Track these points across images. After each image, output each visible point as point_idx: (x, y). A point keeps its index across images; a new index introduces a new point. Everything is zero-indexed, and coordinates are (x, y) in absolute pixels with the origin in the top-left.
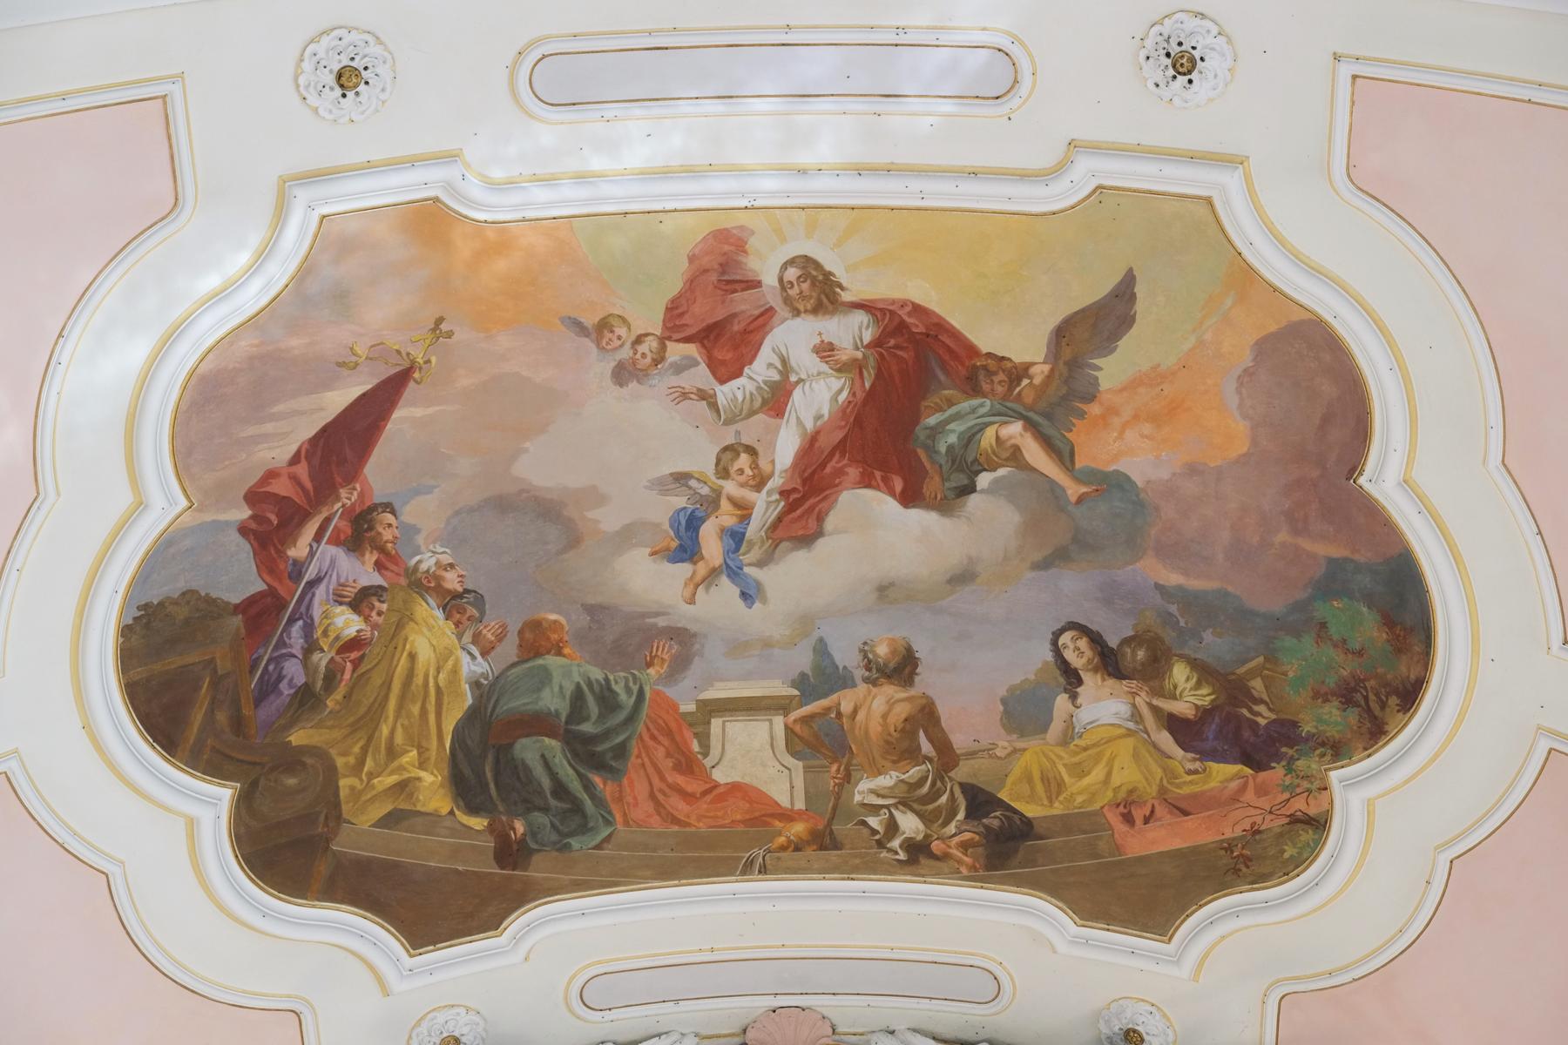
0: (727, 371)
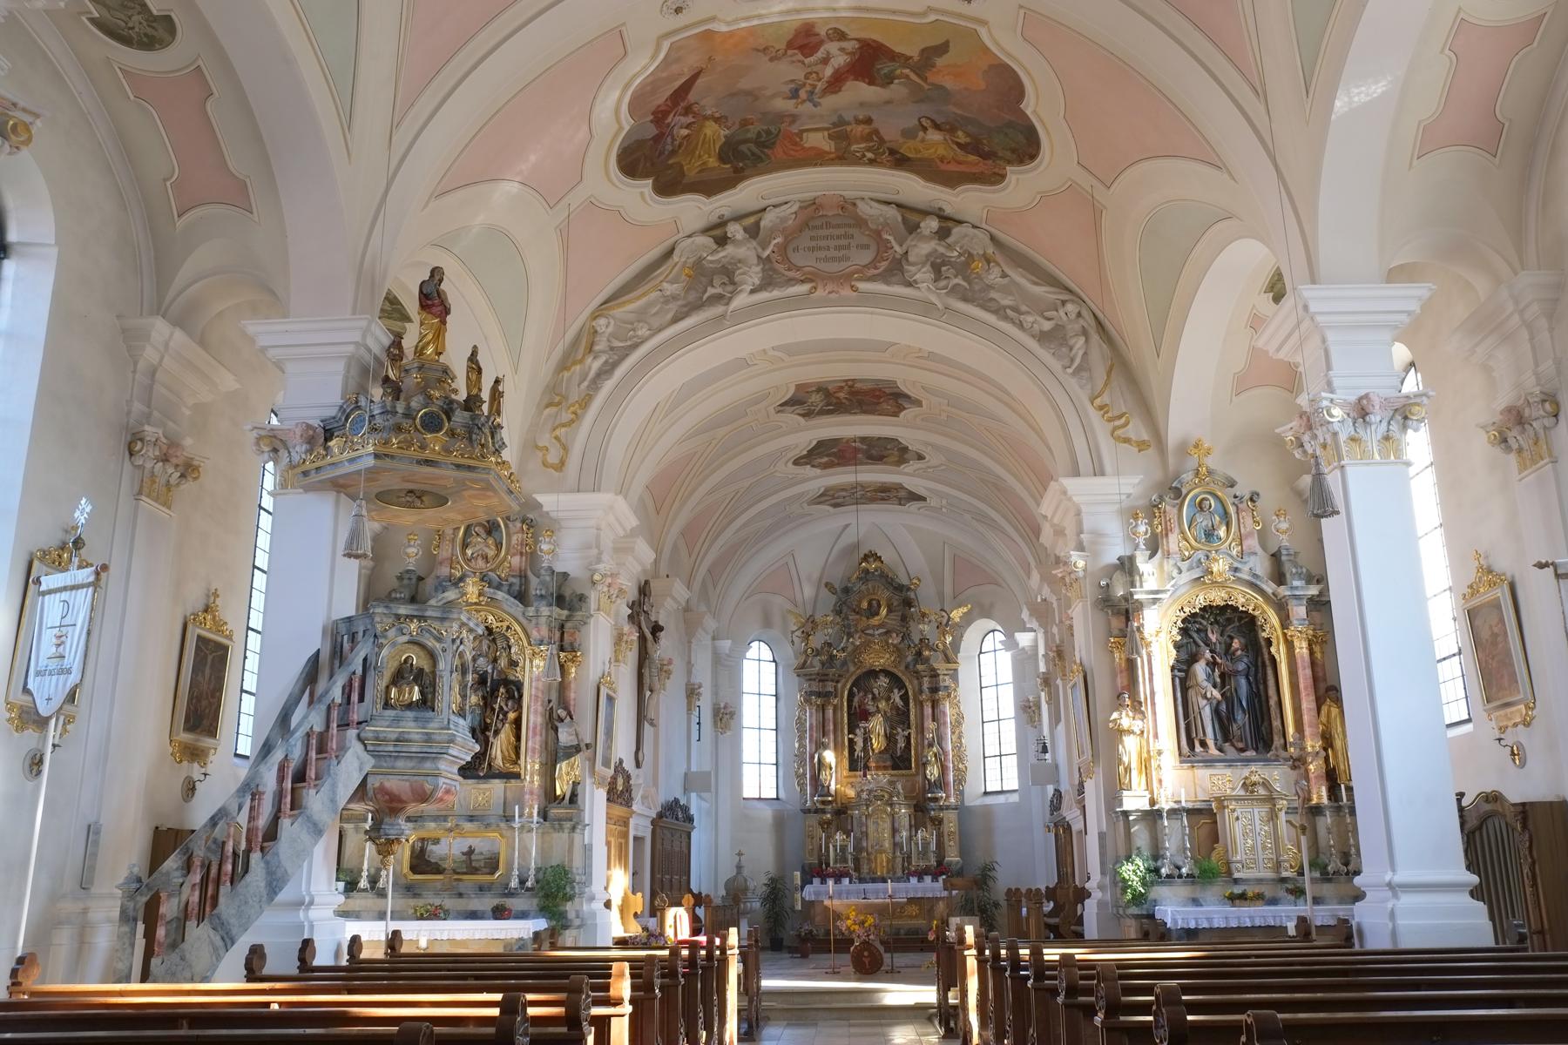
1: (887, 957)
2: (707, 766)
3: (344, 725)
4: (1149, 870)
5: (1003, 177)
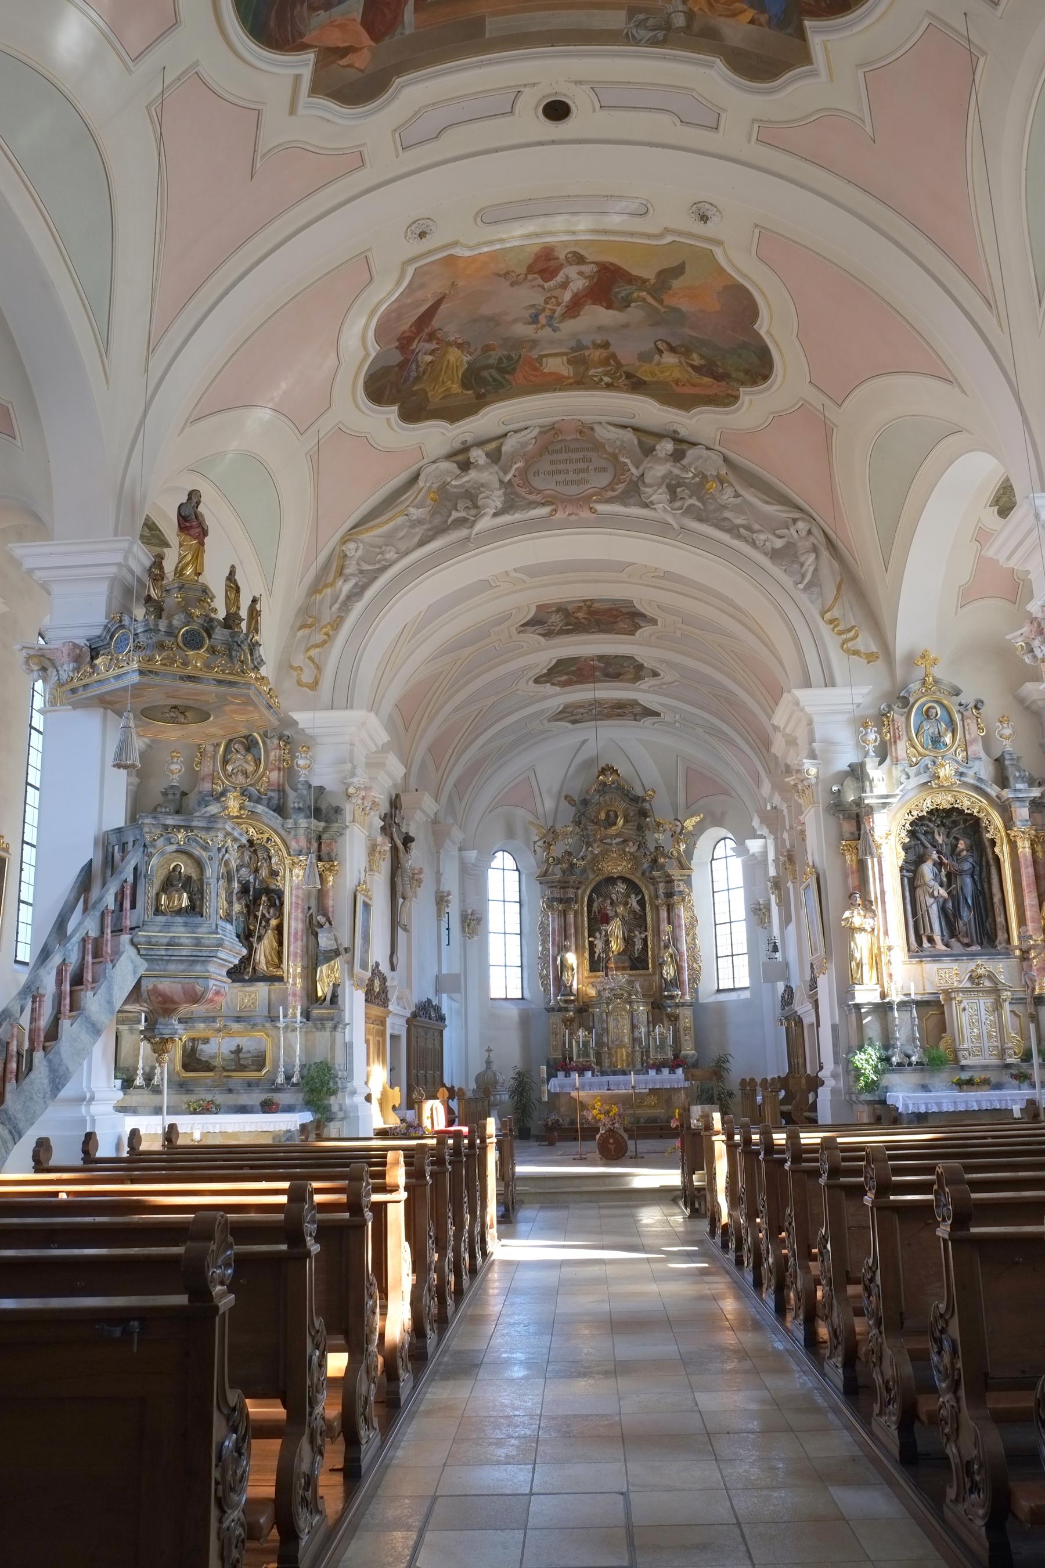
0: (546, 280)
1: (631, 1144)
2: (456, 969)
3: (118, 931)
4: (881, 1059)
5: (736, 398)
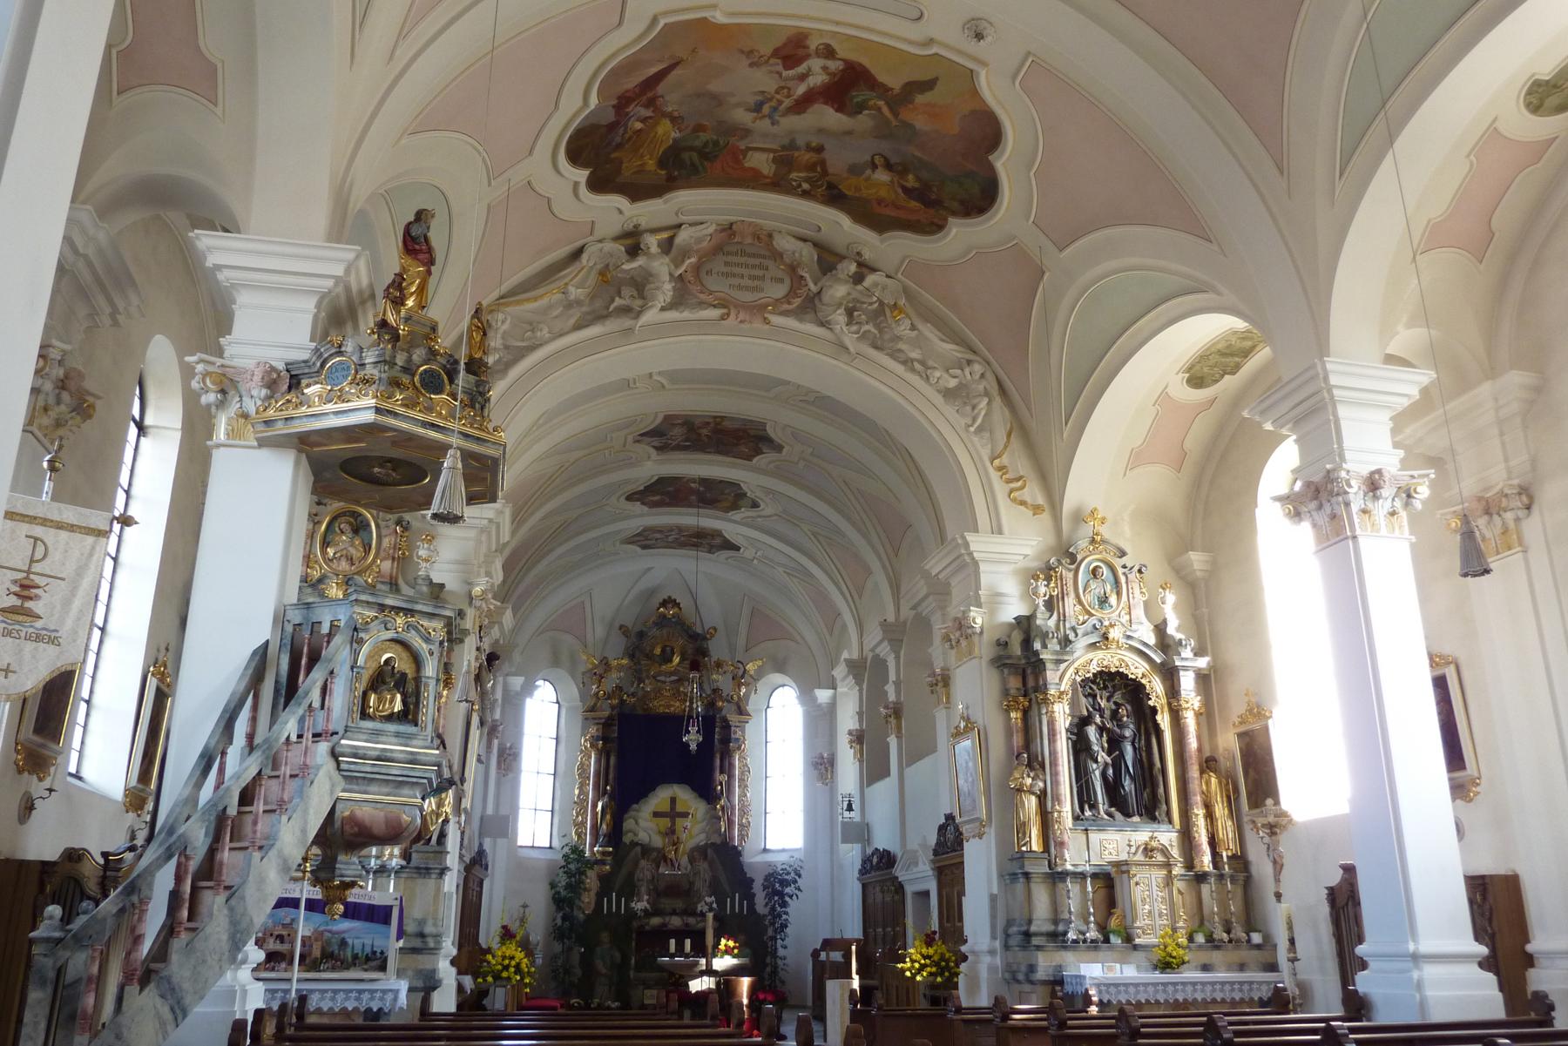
0: (787, 68)
